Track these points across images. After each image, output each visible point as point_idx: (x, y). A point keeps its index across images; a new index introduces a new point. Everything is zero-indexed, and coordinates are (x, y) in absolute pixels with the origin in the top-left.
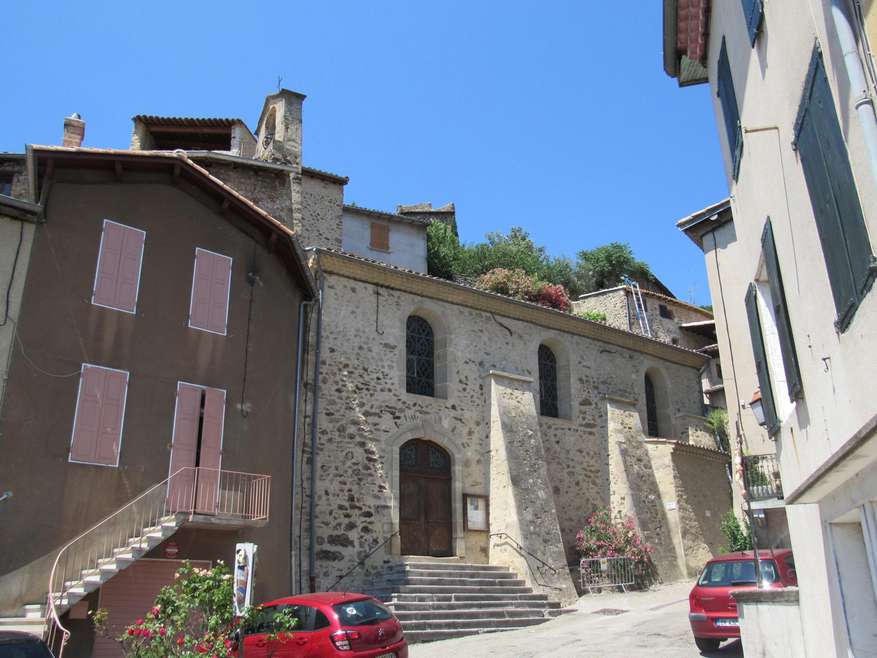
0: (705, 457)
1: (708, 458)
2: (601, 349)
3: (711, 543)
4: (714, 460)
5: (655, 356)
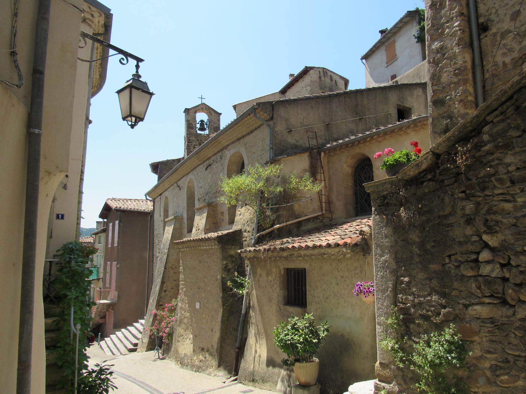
0: (200, 248)
1: (202, 248)
2: (204, 169)
3: (196, 336)
4: (210, 247)
5: (233, 142)
